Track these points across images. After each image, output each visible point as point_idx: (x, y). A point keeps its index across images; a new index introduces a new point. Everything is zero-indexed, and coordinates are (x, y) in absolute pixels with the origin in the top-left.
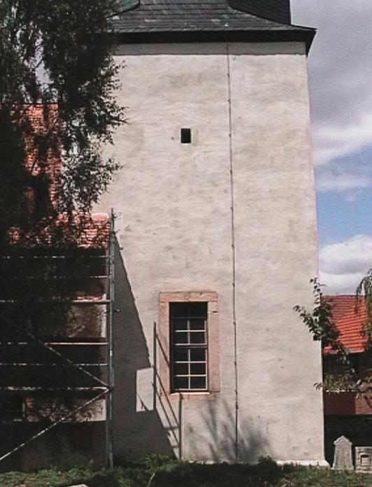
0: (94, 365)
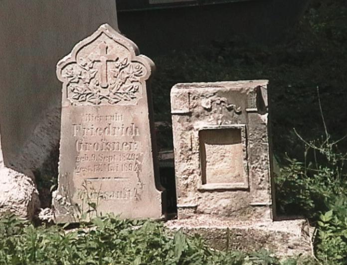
0: (324, 122)
